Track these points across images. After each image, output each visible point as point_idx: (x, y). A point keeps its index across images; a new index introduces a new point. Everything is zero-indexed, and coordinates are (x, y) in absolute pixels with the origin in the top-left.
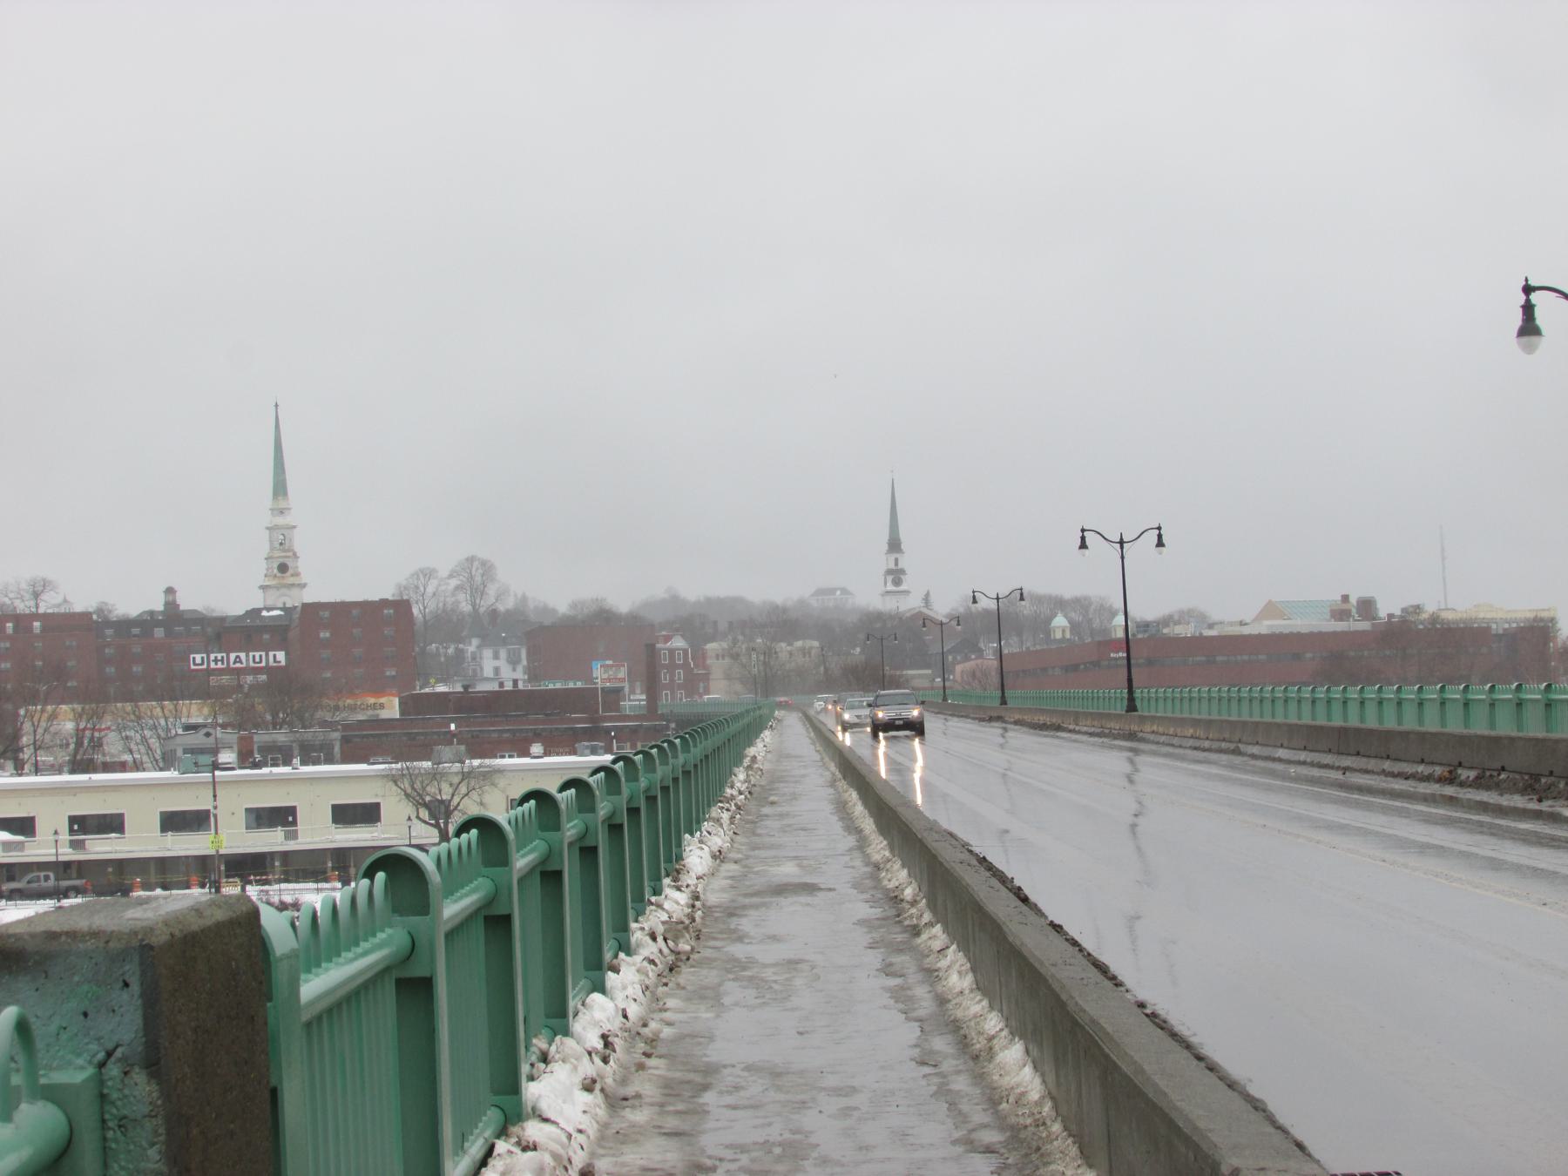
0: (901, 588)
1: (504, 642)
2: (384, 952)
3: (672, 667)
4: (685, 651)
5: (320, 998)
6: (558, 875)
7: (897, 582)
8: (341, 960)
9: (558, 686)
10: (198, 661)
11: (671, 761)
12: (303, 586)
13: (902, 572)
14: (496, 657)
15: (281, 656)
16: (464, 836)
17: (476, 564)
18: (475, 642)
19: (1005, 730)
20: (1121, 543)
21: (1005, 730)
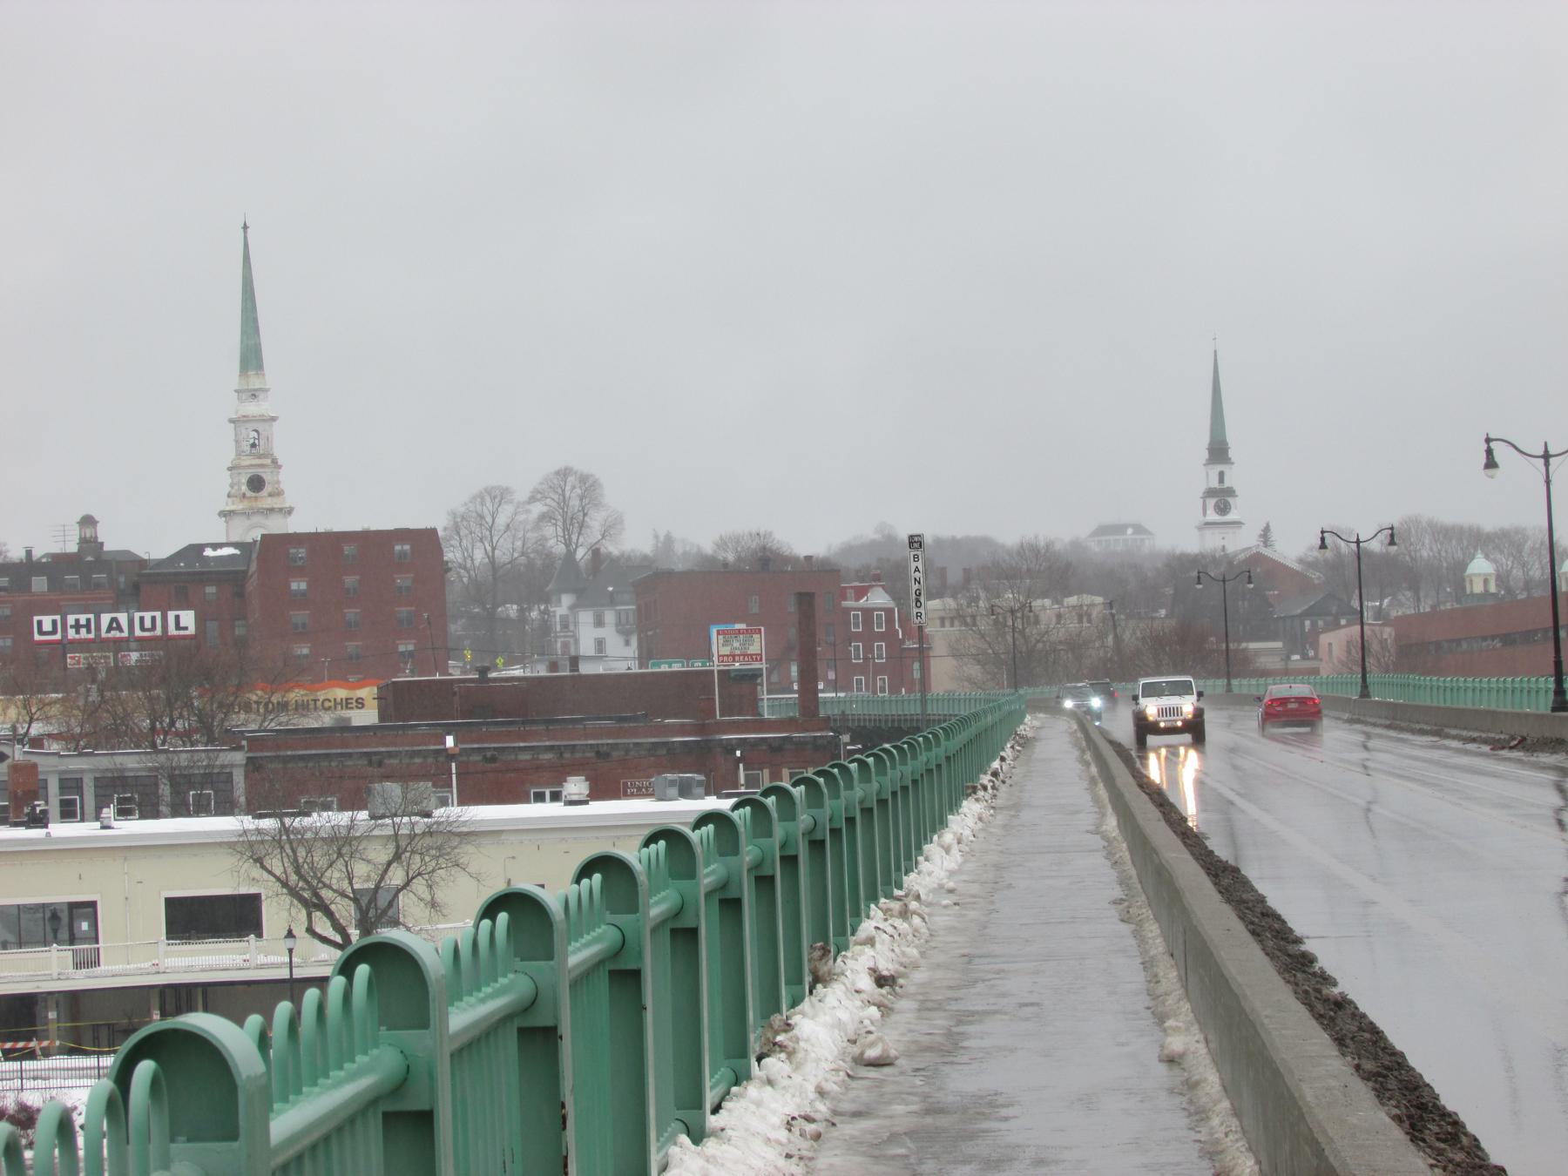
0: (1230, 517)
1: (612, 601)
2: (595, 949)
3: (869, 637)
4: (889, 612)
5: (466, 1029)
6: (693, 933)
7: (1223, 509)
8: (462, 1004)
9: (677, 667)
10: (47, 627)
11: (843, 793)
12: (290, 511)
13: (1230, 492)
14: (599, 622)
15: (188, 618)
16: (653, 846)
17: (571, 479)
18: (567, 600)
19: (1368, 736)
20: (1546, 457)
21: (1368, 736)
